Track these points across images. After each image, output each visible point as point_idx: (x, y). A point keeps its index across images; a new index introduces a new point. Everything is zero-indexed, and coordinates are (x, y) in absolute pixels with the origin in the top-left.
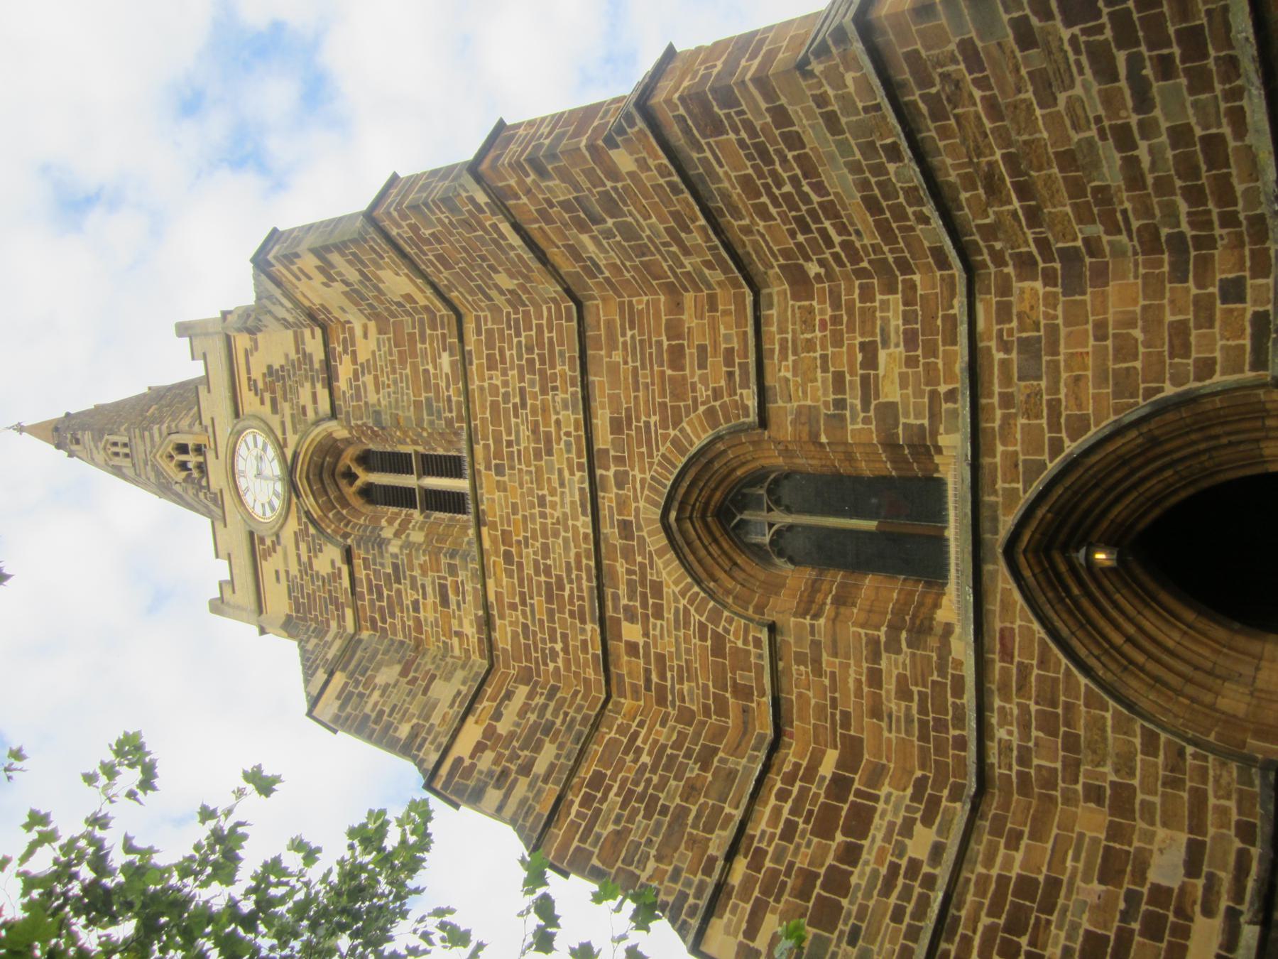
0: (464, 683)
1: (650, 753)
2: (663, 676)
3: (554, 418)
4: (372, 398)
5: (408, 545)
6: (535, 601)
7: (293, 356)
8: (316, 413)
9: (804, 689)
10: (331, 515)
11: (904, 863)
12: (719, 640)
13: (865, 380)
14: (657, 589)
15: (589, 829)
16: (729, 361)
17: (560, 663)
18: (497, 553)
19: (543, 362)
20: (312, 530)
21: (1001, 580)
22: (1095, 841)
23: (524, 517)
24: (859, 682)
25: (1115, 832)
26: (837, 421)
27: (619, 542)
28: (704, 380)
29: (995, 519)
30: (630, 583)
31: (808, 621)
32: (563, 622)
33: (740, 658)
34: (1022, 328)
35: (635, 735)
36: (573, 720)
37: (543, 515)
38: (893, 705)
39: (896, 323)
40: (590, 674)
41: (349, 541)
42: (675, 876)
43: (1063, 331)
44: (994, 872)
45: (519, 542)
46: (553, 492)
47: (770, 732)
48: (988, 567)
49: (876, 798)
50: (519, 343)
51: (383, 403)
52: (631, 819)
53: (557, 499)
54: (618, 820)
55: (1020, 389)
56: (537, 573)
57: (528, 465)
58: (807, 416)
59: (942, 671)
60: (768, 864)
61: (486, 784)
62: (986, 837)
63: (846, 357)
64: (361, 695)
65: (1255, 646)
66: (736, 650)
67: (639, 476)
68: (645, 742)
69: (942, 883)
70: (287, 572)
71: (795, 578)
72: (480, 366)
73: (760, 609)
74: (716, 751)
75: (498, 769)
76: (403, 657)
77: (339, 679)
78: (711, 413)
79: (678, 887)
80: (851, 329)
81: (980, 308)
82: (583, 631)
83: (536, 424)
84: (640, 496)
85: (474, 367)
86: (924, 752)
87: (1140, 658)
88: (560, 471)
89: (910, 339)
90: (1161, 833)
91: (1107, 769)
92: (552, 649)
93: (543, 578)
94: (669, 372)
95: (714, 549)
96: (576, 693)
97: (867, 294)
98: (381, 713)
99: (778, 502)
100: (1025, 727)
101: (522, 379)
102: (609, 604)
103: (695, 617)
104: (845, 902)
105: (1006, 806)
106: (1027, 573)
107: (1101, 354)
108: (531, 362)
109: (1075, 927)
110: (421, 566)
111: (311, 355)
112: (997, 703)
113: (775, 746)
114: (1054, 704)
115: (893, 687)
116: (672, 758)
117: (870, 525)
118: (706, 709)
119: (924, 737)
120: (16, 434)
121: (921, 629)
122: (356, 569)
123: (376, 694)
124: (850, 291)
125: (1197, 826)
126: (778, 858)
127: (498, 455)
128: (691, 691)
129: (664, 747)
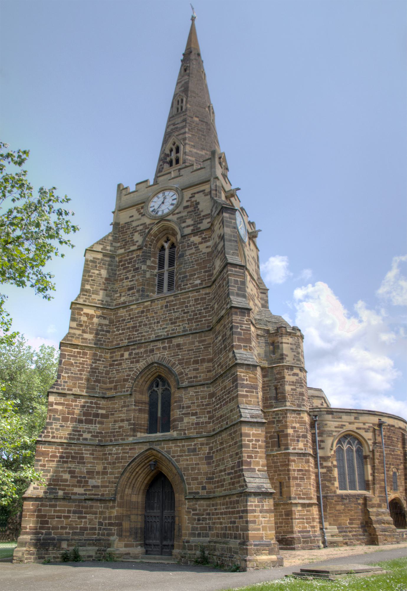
0: (106, 301)
1: (95, 366)
2: (117, 365)
3: (181, 324)
4: (188, 253)
5: (145, 271)
6: (132, 323)
7: (203, 214)
8: (184, 228)
9: (118, 404)
10: (152, 237)
11: (81, 433)
12: (126, 380)
13: (189, 413)
14: (138, 362)
15: (71, 356)
16: (196, 377)
17: (116, 333)
18: (144, 308)
19: (197, 318)
20: (147, 231)
21: (145, 447)
22: (95, 469)
23: (154, 317)
24: (121, 417)
25: (98, 473)
26: (180, 407)
27: (148, 348)
28: (190, 371)
29: (158, 445)
30: (138, 353)
31: (133, 403)
32: (127, 332)
33: (123, 386)
34: (198, 448)
35: (100, 360)
36: (101, 341)
37: (155, 323)
38: (117, 425)
39: (202, 420)
40: (115, 343)
41: (144, 248)
42: (66, 382)
43: (197, 457)
44: (84, 452)
45: (147, 315)
46: (161, 326)
47: (107, 396)
48: (148, 444)
49: (95, 424)
50: (201, 310)
51: (186, 258)
52: (77, 366)
53: (159, 328)
54: (75, 363)
55: (186, 448)
56: (139, 323)
57: (168, 317)
58: (180, 400)
59: (126, 436)
60: (74, 403)
61: (77, 321)
62: (91, 449)
63: (194, 408)
64: (96, 266)
65: (141, 493)
66: (125, 385)
67: (165, 353)
68: (98, 364)
69: (79, 442)
70: (133, 221)
71: (145, 398)
72: (195, 296)
73: (135, 391)
74: (100, 383)
75: (82, 323)
76: (111, 277)
77: (100, 256)
78: (182, 373)
79: (63, 384)
80: (201, 409)
81: (203, 439)
82: (125, 339)
83: (179, 318)
84: (162, 354)
85: (195, 294)
86: (108, 433)
87: (134, 474)
88: (166, 328)
89: (197, 424)
90: (100, 481)
91: (110, 470)
92: (119, 330)
93: (138, 325)
94: (192, 360)
95: (150, 376)
96: (109, 339)
97: (209, 412)
98: (91, 276)
99: (164, 391)
100: (116, 454)
101: (192, 312)
102: (133, 347)
103: (132, 373)
104: (69, 423)
105: (99, 451)
106: (147, 452)
107: (193, 464)
108: (196, 314)
109: (76, 468)
110: (138, 279)
111: (202, 223)
112: (120, 448)
113: (103, 398)
114: (122, 459)
115: (121, 425)
116: (95, 372)
117: (159, 414)
118: (110, 378)
119: (111, 432)
120: (190, 17)
121: (134, 430)
122: (136, 252)
123: (97, 272)
124: (210, 408)
125: (102, 487)
126: (76, 406)
127: (171, 305)
128: (114, 373)
129: (98, 369)
